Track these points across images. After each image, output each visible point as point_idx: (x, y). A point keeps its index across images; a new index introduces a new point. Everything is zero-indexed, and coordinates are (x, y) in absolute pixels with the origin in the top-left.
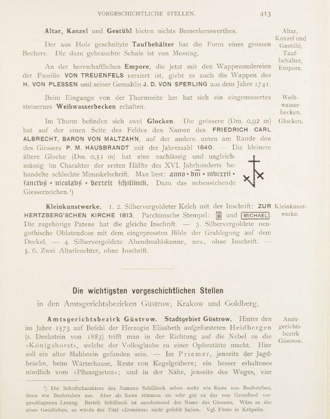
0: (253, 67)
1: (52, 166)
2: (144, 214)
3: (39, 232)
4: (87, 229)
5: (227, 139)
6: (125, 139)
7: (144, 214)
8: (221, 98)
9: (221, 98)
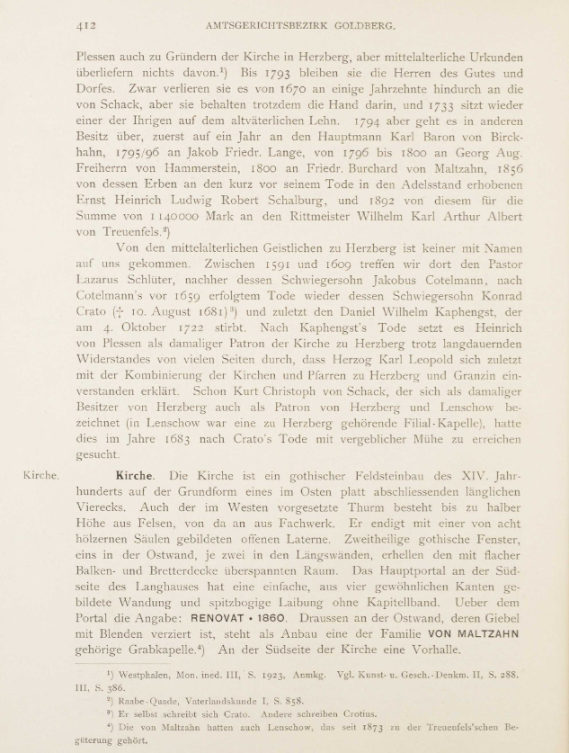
0: (427, 58)
1: (113, 440)
2: (493, 262)
3: (446, 537)
4: (162, 532)
5: (186, 344)
6: (494, 634)
7: (493, 262)
8: (397, 728)
9: (397, 728)
